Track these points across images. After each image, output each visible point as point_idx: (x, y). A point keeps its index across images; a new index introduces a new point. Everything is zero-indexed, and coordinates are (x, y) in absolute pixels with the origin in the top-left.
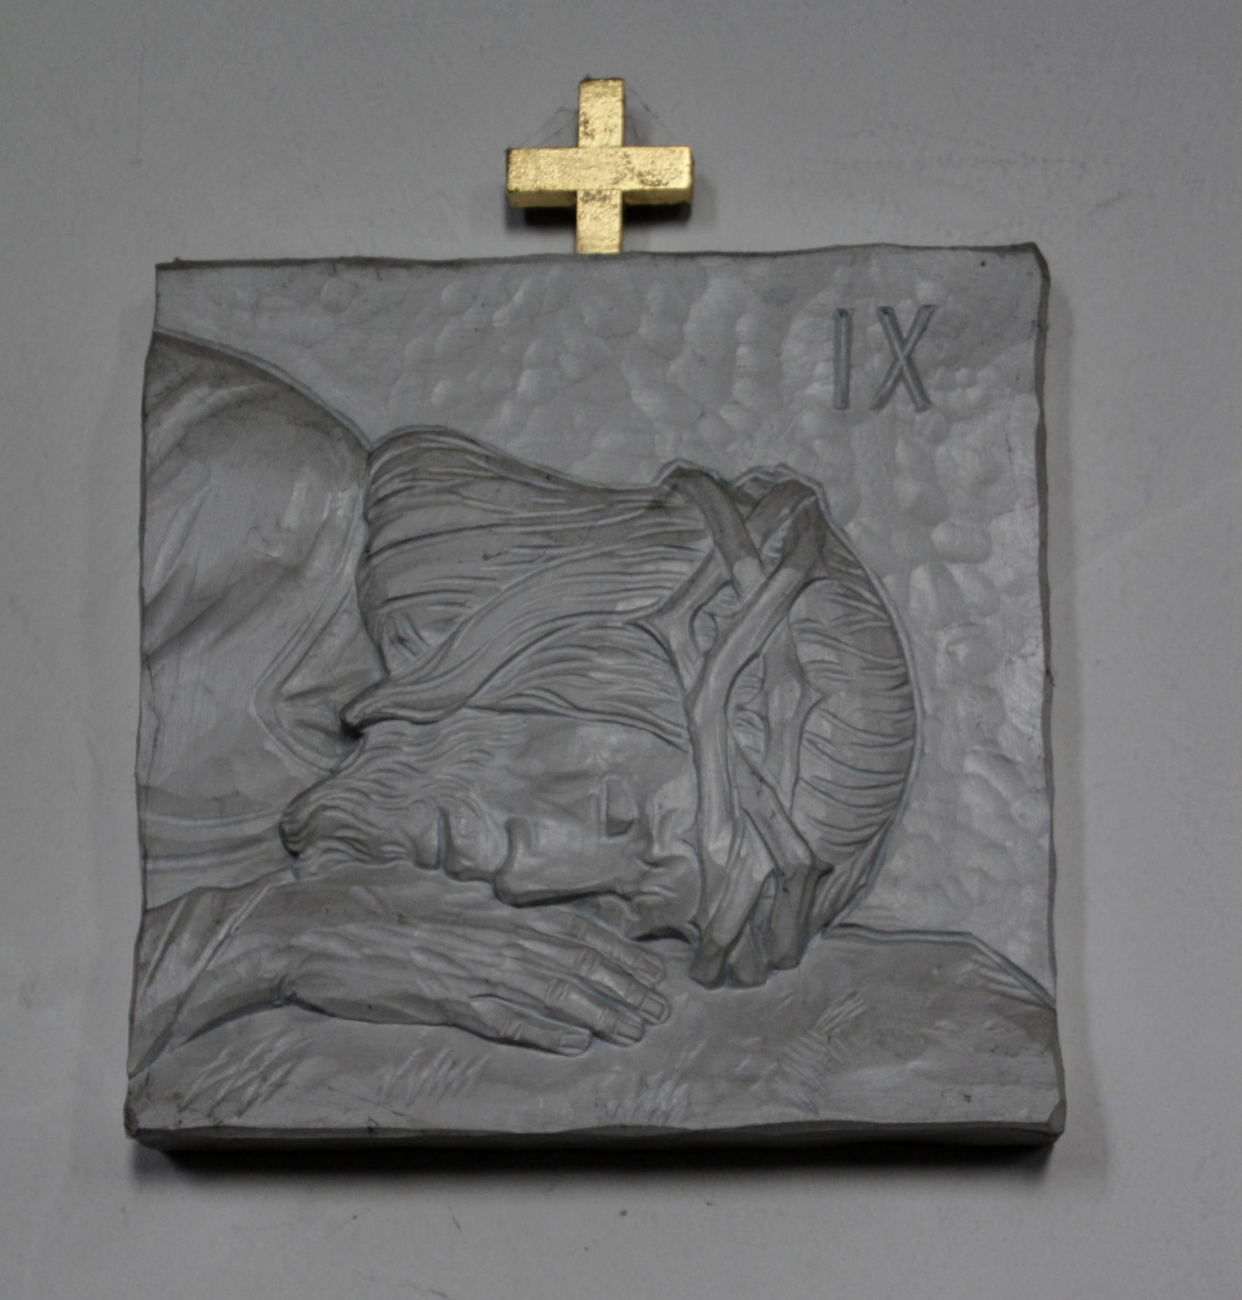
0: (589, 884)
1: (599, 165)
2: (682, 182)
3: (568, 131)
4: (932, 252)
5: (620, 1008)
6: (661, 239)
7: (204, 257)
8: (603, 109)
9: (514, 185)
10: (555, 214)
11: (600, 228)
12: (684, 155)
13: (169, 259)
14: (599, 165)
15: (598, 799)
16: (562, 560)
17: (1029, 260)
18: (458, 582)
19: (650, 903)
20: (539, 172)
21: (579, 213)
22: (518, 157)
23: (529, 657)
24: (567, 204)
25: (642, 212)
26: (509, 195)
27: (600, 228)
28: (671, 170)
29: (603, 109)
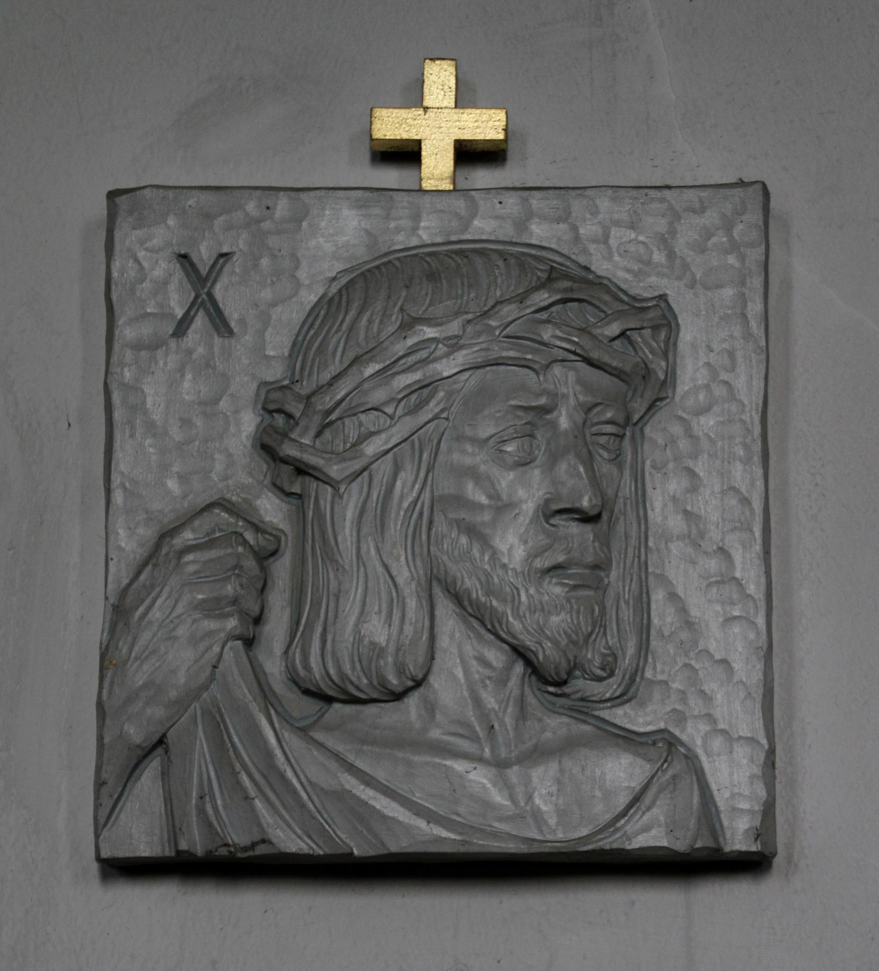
1: (440, 121)
3: (413, 96)
4: (518, 185)
6: (482, 177)
8: (439, 80)
10: (407, 154)
11: (437, 166)
12: (499, 116)
13: (771, 188)
14: (440, 121)
16: (342, 345)
17: (122, 200)
18: (310, 533)
20: (392, 125)
23: (397, 605)
24: (416, 149)
25: (467, 154)
27: (437, 166)
28: (486, 125)
29: (439, 80)
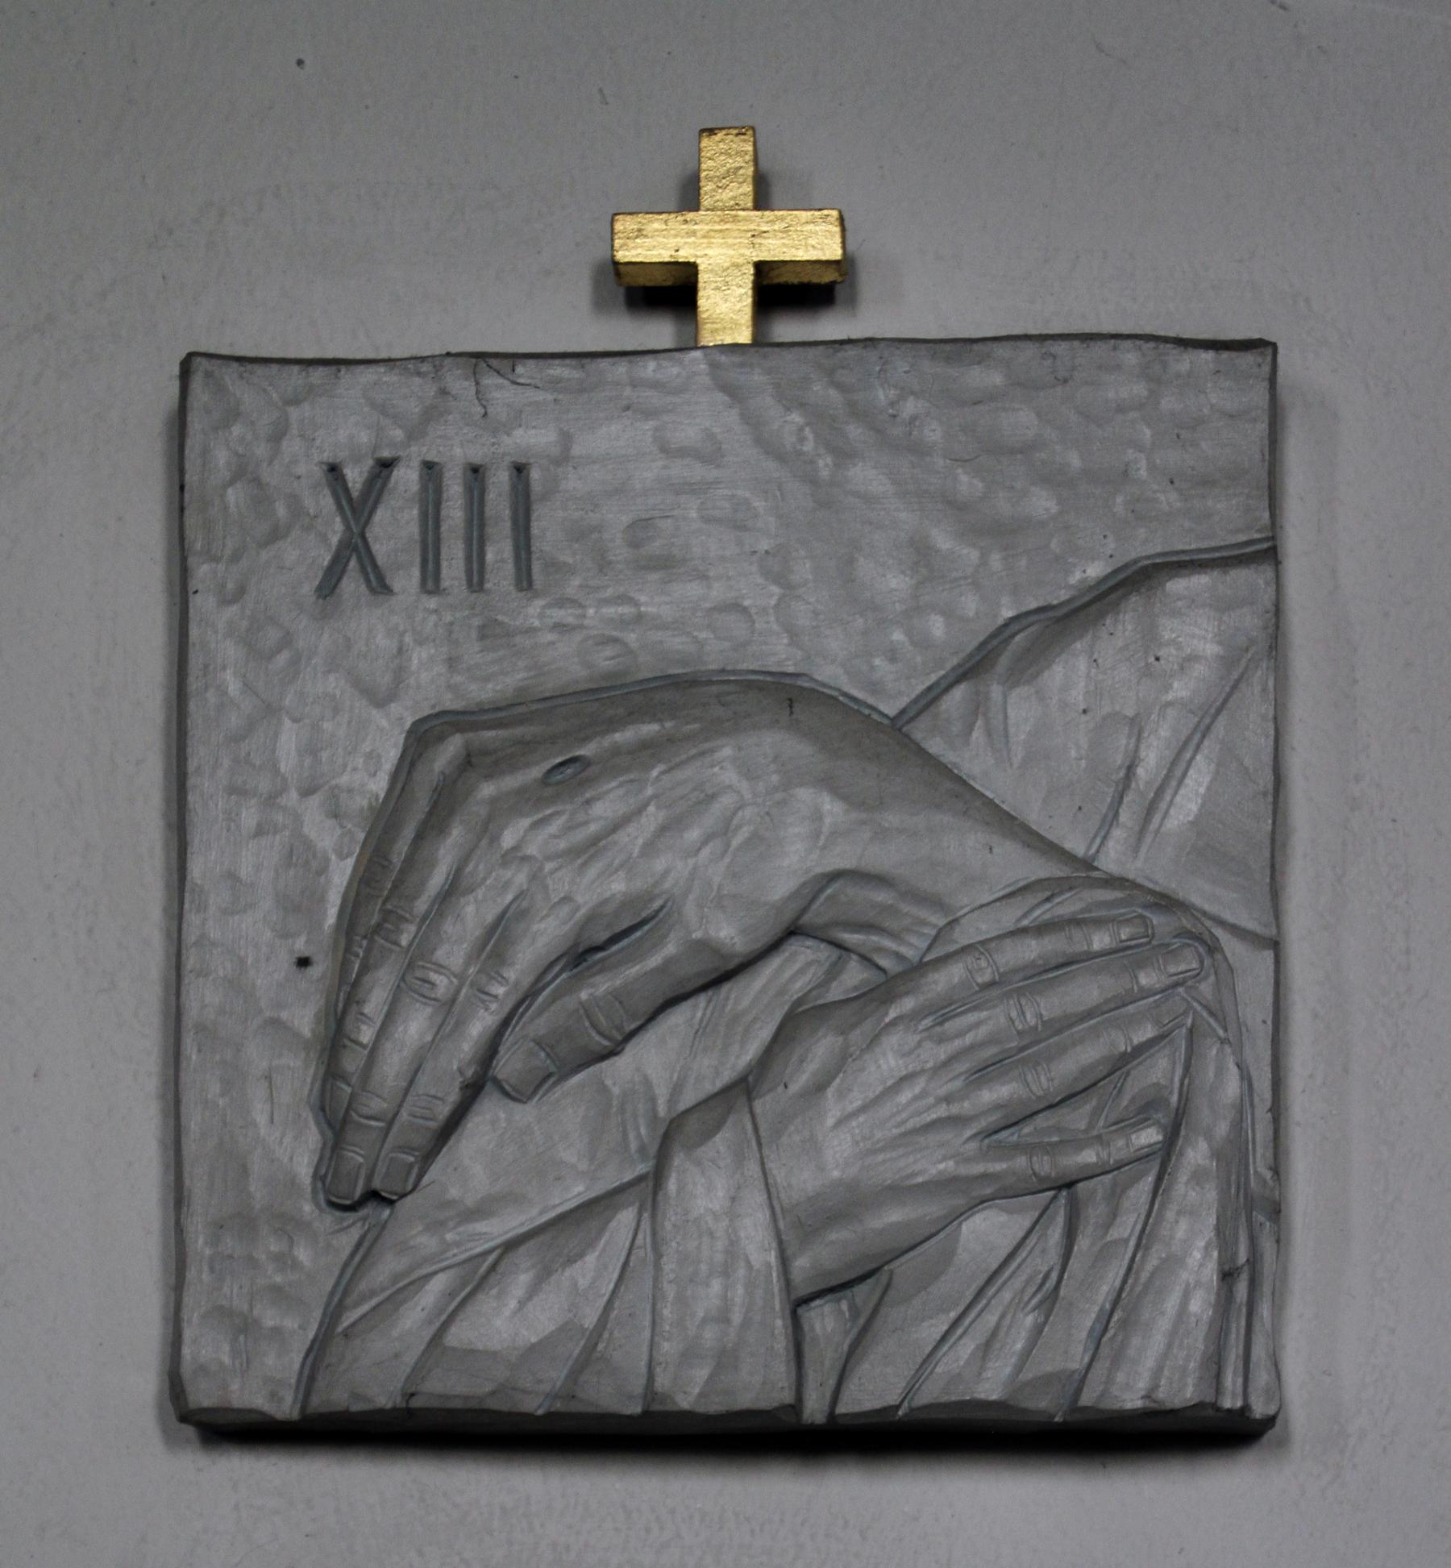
0: (776, 1290)
1: (723, 252)
2: (834, 252)
5: (735, 822)
7: (360, 356)
8: (725, 162)
9: (622, 256)
10: (672, 292)
11: (726, 308)
14: (723, 252)
15: (577, 909)
18: (1024, 1254)
19: (1050, 1232)
20: (651, 242)
21: (701, 285)
22: (623, 224)
25: (779, 291)
26: (618, 268)
27: (726, 308)
29: (725, 162)
